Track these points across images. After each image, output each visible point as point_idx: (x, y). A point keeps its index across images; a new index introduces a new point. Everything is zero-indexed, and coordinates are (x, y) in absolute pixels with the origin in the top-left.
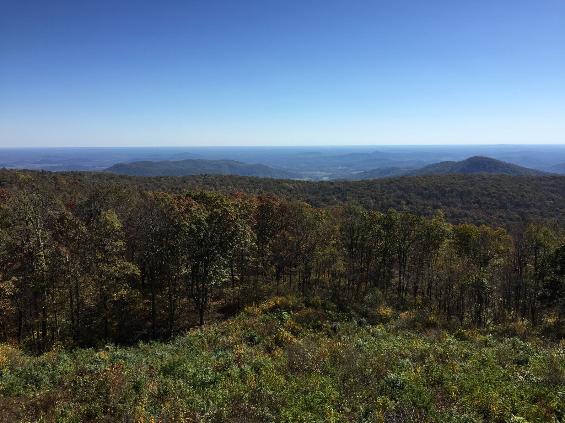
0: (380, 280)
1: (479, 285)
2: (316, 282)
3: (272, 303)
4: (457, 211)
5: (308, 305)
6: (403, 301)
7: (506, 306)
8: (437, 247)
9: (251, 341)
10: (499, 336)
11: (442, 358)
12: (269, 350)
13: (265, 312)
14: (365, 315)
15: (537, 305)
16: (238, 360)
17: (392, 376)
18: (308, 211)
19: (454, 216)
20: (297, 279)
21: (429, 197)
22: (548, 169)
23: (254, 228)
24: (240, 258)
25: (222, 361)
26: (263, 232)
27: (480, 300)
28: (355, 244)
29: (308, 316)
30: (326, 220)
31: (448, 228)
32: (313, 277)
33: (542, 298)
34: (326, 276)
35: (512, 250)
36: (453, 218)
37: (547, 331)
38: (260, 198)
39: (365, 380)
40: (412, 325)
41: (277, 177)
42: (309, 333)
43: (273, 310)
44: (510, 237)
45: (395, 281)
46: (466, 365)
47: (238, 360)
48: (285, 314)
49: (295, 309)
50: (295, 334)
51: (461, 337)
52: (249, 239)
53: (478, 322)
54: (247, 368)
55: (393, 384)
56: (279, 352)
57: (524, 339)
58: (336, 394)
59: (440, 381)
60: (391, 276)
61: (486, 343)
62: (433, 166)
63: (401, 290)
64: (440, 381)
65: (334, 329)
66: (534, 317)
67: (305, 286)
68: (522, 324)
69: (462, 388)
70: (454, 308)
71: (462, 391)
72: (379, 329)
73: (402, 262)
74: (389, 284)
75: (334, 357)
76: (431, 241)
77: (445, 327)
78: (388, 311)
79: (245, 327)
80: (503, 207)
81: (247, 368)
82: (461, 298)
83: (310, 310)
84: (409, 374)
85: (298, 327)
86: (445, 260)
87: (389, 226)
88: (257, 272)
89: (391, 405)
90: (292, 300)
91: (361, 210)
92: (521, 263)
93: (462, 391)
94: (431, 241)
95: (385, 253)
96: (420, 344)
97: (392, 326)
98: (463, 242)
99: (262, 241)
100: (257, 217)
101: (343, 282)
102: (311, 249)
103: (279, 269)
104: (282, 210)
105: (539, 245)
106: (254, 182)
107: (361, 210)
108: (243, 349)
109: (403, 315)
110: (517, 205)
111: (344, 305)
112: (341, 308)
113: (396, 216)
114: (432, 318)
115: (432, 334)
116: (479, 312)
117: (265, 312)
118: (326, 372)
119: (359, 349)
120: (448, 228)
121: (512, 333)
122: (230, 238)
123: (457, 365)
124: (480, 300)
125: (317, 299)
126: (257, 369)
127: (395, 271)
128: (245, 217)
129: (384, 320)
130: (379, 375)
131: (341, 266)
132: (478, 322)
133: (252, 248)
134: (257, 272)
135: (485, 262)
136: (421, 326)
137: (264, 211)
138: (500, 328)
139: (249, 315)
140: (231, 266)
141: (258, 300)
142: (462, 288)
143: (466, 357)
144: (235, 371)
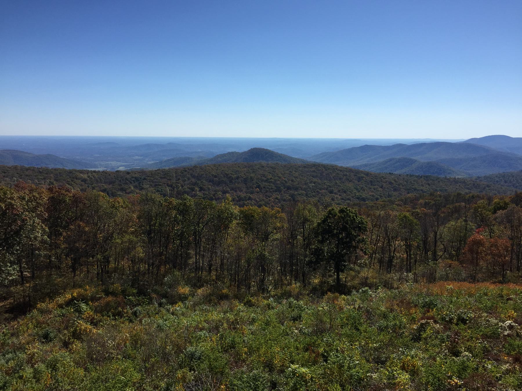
0: (178, 262)
1: (262, 257)
2: (115, 270)
3: (68, 296)
4: (243, 195)
5: (107, 293)
6: (199, 279)
7: (283, 273)
8: (227, 227)
9: (46, 338)
10: (278, 299)
11: (233, 325)
12: (66, 345)
13: (61, 306)
14: (165, 296)
15: (306, 269)
16: (31, 360)
17: (190, 349)
18: (104, 201)
19: (240, 199)
20: (95, 270)
21: (219, 184)
22: (310, 159)
23: (44, 221)
24: (30, 253)
25: (11, 364)
26: (54, 225)
27: (264, 271)
28: (153, 230)
29: (108, 304)
30: (124, 208)
31: (236, 210)
32: (112, 265)
33: (310, 262)
34: (125, 263)
35: (286, 225)
36: (239, 201)
37: (314, 290)
38: (50, 190)
39: (166, 357)
40: (208, 300)
41: (69, 167)
42: (109, 321)
43: (69, 303)
44: (284, 215)
45: (191, 261)
46: (254, 328)
47: (31, 360)
48: (83, 306)
49: (93, 299)
50: (94, 323)
51: (249, 304)
52: (40, 233)
53: (262, 289)
54: (42, 367)
55: (192, 356)
56: (77, 345)
57: (297, 298)
58: (137, 376)
59: (233, 346)
60: (188, 256)
61: (269, 307)
62: (218, 156)
63: (197, 269)
64: (233, 346)
65: (135, 314)
66: (304, 279)
67: (104, 275)
68: (296, 286)
69: (250, 348)
70: (242, 280)
71: (251, 351)
72: (179, 307)
73: (197, 243)
74: (186, 265)
75: (136, 341)
76: (222, 222)
77: (237, 297)
78: (185, 290)
79: (39, 324)
80: (278, 190)
81: (42, 367)
82: (248, 271)
83: (110, 298)
84: (206, 345)
85: (97, 317)
86: (234, 239)
87: (184, 211)
88: (50, 266)
89: (190, 376)
90: (90, 290)
91: (158, 197)
92: (293, 236)
93: (251, 351)
94: (222, 222)
95: (181, 236)
96: (215, 315)
97: (189, 303)
98: (248, 222)
99: (54, 233)
100: (48, 210)
101: (143, 267)
102: (109, 238)
103: (75, 261)
104: (76, 200)
105: (306, 220)
106: (43, 174)
107: (158, 197)
108: (37, 348)
109: (200, 291)
110: (289, 188)
111: (147, 288)
112: (141, 292)
113: (191, 201)
114: (225, 291)
115: (225, 304)
116: (262, 281)
117: (61, 306)
118: (127, 357)
119: (160, 328)
120: (236, 210)
121: (288, 295)
122: (17, 233)
123: (247, 329)
124: (264, 271)
125: (117, 286)
126: (53, 366)
127: (192, 252)
128: (34, 210)
129: (183, 298)
130: (179, 349)
131: (140, 252)
132: (262, 289)
133: (43, 242)
134: (50, 266)
135: (266, 237)
136: (216, 299)
137: (55, 203)
138: (279, 291)
139: (42, 312)
140: (19, 262)
141: (51, 295)
142: (248, 262)
143: (253, 321)
144: (28, 372)
